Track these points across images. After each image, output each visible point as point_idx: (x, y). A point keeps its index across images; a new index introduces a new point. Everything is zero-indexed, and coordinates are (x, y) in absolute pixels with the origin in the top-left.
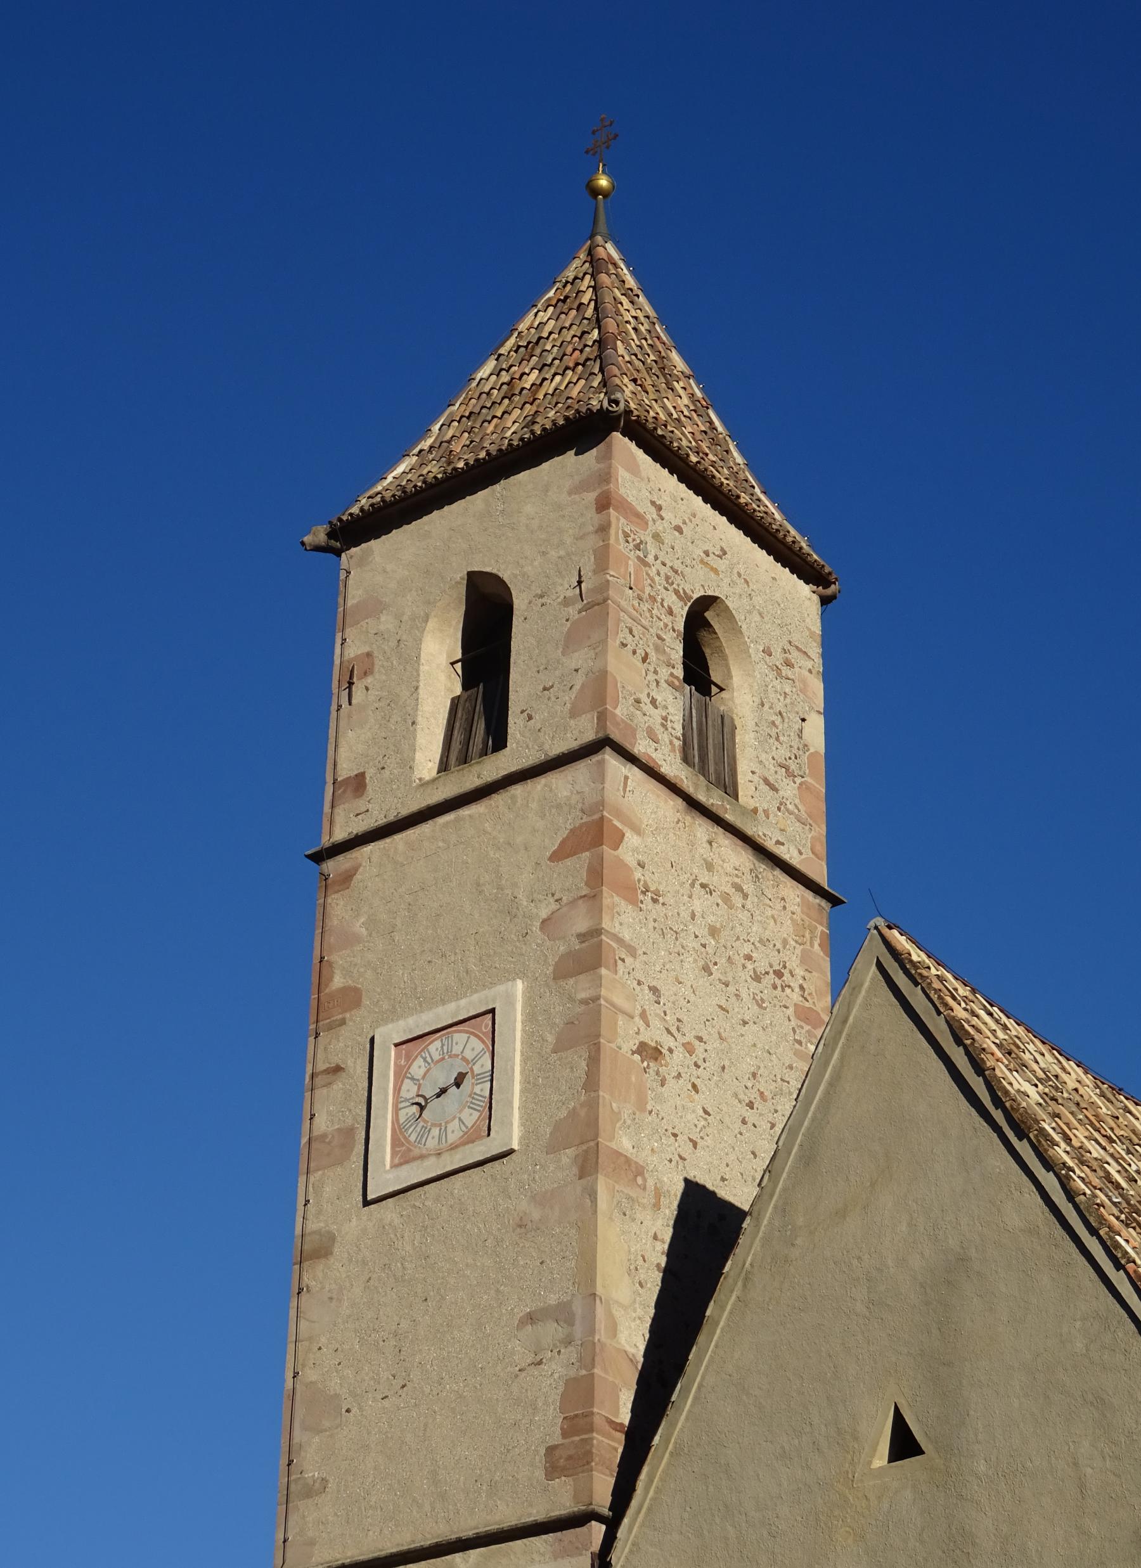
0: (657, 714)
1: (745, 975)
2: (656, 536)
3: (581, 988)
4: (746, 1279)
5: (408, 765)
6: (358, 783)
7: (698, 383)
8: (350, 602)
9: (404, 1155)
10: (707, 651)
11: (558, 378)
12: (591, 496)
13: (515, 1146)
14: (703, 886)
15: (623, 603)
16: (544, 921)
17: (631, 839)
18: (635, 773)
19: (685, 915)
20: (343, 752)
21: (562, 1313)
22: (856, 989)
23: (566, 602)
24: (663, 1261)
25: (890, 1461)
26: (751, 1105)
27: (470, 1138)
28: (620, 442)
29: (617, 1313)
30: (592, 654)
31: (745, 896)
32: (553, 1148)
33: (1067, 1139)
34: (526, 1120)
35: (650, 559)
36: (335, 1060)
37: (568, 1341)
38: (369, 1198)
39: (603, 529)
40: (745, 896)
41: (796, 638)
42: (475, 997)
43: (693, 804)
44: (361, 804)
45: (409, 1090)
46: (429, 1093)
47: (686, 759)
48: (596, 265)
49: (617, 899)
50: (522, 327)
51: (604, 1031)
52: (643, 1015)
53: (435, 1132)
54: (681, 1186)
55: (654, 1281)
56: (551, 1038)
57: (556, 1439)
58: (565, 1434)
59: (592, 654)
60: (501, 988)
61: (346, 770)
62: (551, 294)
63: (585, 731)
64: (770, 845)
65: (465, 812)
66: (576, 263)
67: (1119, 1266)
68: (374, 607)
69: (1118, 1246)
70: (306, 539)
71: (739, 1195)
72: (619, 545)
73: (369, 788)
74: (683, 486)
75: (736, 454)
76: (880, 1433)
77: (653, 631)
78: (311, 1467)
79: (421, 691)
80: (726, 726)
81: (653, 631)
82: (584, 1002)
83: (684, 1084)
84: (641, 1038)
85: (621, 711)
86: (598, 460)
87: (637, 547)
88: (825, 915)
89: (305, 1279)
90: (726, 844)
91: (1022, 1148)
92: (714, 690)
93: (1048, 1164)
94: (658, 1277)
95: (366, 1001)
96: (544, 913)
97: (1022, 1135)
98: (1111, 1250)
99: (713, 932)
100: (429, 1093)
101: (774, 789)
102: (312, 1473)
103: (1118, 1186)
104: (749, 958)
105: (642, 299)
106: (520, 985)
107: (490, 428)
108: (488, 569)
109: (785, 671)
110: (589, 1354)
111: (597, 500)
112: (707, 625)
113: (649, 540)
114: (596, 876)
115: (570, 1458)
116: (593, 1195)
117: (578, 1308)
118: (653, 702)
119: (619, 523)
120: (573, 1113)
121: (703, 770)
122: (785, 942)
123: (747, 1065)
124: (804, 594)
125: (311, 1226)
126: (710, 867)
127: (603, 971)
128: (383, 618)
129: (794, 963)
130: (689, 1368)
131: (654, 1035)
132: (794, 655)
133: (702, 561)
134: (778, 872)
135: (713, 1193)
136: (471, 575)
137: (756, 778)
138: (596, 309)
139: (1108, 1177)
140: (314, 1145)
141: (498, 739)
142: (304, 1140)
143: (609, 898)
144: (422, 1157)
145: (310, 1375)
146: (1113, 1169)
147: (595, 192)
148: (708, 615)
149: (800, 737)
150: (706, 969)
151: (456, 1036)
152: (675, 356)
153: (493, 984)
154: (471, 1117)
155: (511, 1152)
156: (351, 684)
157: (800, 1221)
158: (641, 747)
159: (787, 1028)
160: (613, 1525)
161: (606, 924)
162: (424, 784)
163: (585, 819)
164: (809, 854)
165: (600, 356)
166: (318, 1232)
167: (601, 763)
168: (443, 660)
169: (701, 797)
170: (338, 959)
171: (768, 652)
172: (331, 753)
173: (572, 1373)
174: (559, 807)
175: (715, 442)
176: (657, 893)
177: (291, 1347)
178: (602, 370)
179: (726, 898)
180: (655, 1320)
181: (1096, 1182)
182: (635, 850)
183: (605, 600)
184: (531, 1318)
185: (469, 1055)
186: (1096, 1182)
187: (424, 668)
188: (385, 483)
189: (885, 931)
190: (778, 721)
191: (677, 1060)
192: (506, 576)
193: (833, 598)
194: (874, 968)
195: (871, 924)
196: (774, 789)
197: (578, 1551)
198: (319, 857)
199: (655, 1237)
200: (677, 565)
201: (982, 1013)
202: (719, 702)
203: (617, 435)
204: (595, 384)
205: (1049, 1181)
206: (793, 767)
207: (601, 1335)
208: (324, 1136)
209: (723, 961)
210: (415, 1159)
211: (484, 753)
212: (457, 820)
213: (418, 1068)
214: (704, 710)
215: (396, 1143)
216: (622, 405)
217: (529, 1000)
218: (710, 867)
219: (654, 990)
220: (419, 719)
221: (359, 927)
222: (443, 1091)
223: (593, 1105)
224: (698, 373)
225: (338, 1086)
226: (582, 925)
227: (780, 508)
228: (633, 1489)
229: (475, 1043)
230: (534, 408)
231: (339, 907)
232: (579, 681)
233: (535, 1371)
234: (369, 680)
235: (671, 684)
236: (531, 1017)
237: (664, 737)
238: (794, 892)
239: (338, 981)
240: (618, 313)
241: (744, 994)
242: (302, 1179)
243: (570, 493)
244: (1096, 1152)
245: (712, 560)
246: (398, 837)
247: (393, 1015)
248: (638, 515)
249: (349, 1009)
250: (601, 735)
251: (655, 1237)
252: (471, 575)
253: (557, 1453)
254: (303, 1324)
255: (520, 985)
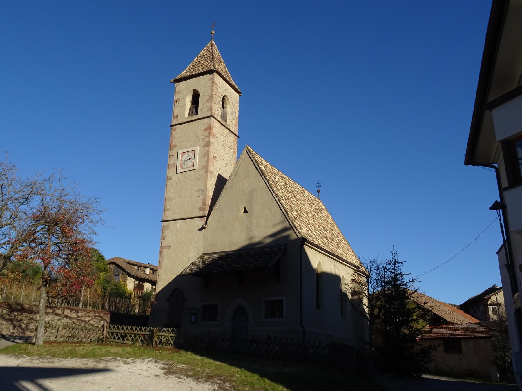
0: (218, 112)
1: (227, 147)
2: (219, 87)
3: (207, 148)
4: (227, 189)
5: (184, 115)
6: (177, 117)
7: (225, 63)
8: (176, 91)
9: (182, 168)
10: (224, 102)
11: (207, 62)
12: (211, 81)
13: (197, 168)
14: (222, 135)
15: (215, 97)
16: (202, 139)
17: (214, 129)
18: (215, 120)
19: (220, 139)
20: (175, 112)
21: (202, 190)
22: (243, 154)
23: (207, 96)
24: (215, 184)
25: (244, 213)
26: (227, 164)
27: (191, 167)
28: (215, 73)
29: (209, 191)
30: (210, 103)
31: (227, 136)
32: (202, 169)
33: (268, 175)
34: (198, 165)
35: (218, 90)
36: (173, 154)
37: (203, 194)
38: (177, 173)
39: (213, 86)
40: (227, 136)
41: (236, 101)
42: (192, 148)
43: (222, 124)
44: (177, 120)
45: (183, 159)
46: (186, 160)
47: (221, 118)
48: (212, 45)
49: (212, 137)
50: (201, 53)
51: (210, 154)
52: (214, 152)
53: (186, 165)
54: (218, 175)
55: (214, 187)
56: (202, 155)
57: (201, 206)
58: (202, 206)
59: (210, 103)
60: (196, 147)
61: (175, 115)
62: (205, 48)
63: (208, 114)
64: (231, 130)
65: (192, 123)
66: (209, 44)
67: (274, 192)
68: (180, 92)
69: (274, 190)
70: (171, 81)
71: (226, 176)
72: (215, 89)
73: (178, 118)
74: (223, 80)
75: (229, 74)
76: (243, 209)
77: (218, 100)
78: (168, 206)
79: (186, 105)
80: (226, 113)
81: (218, 100)
82: (207, 150)
83: (219, 161)
84: (214, 155)
85: (214, 112)
86: (212, 76)
87: (217, 89)
88: (237, 139)
89: (168, 183)
90: (226, 129)
91: (263, 176)
92: (225, 108)
93: (266, 179)
94: (214, 186)
95: (177, 147)
96: (202, 138)
97: (263, 175)
98: (273, 190)
99: (223, 141)
100: (186, 160)
101: (232, 122)
102: (168, 208)
103: (274, 181)
104: (227, 145)
105: (218, 50)
106: (198, 147)
107: (197, 68)
108: (196, 89)
109: (234, 106)
110: (206, 196)
111: (212, 82)
112: (225, 99)
113: (218, 87)
114: (209, 134)
115: (202, 209)
116: (207, 176)
117: (204, 190)
118: (218, 110)
119: (215, 85)
120: (205, 165)
121: (223, 119)
122: (232, 143)
123: (226, 159)
124: (237, 95)
125: (169, 176)
126: (223, 132)
127: (210, 147)
128: (181, 94)
129: (233, 145)
130: (219, 199)
131: (216, 155)
132: (235, 104)
133: (225, 91)
134: (232, 133)
135: (221, 176)
136: (194, 90)
137: (230, 121)
138: (212, 52)
139: (273, 180)
140: (169, 165)
141: (197, 113)
142: (168, 164)
143: (211, 137)
144: (184, 168)
145: (168, 195)
146: (273, 179)
147: (212, 33)
148: (225, 98)
149: (235, 115)
150: (222, 146)
151: (190, 153)
152: (222, 59)
153: (195, 147)
154: (191, 164)
155: (196, 169)
156: (176, 102)
157: (234, 182)
158: (216, 117)
159: (232, 154)
160: (208, 217)
161: (210, 140)
162: (186, 118)
163: (209, 126)
164: (235, 130)
165: (212, 60)
166: (170, 177)
167: (211, 118)
168: (189, 101)
169: (223, 123)
170: (173, 140)
171: (232, 103)
172: (173, 112)
173: (203, 198)
174: (205, 124)
175: (227, 73)
176: (217, 136)
177: (166, 191)
178: (213, 62)
179: (225, 137)
180: (214, 192)
181: (271, 181)
182: (214, 130)
183: (212, 96)
184: (198, 191)
185: (191, 156)
186: (271, 181)
187: (187, 102)
188: (182, 74)
189: (248, 147)
190: (233, 112)
191: (218, 158)
192: (199, 90)
193: (241, 95)
194: (246, 151)
195: (246, 145)
196: (232, 122)
197: (203, 220)
198: (171, 126)
199: (214, 181)
200: (222, 91)
201: (258, 157)
202: (225, 109)
203: (215, 73)
204: (212, 64)
205: (266, 181)
206: (234, 119)
207: (207, 194)
208: (171, 164)
209: (224, 145)
210: (183, 168)
211: (195, 115)
212: (191, 123)
213: (184, 156)
214: (224, 111)
215: (181, 166)
216: (216, 69)
217: (200, 149)
218: (223, 132)
219: (216, 149)
220: (186, 109)
221: (176, 136)
222: (188, 160)
223: (208, 164)
224: (225, 62)
225: (173, 157)
226: (207, 140)
227: (235, 82)
228: (210, 214)
229: (192, 154)
230: (203, 66)
231: (174, 133)
232: (208, 107)
233: (199, 197)
234: (179, 102)
235: (220, 108)
236: (200, 152)
237: (219, 115)
238: (233, 136)
239: (173, 143)
240: (215, 53)
241: (226, 149)
242: (168, 169)
243: (208, 80)
244: (271, 176)
245: (226, 90)
246: (182, 125)
247: (181, 149)
248: (217, 84)
249: (174, 147)
250: (211, 115)
251: (214, 181)
252: (194, 90)
253: (201, 208)
254: (167, 188)
255: (198, 147)
